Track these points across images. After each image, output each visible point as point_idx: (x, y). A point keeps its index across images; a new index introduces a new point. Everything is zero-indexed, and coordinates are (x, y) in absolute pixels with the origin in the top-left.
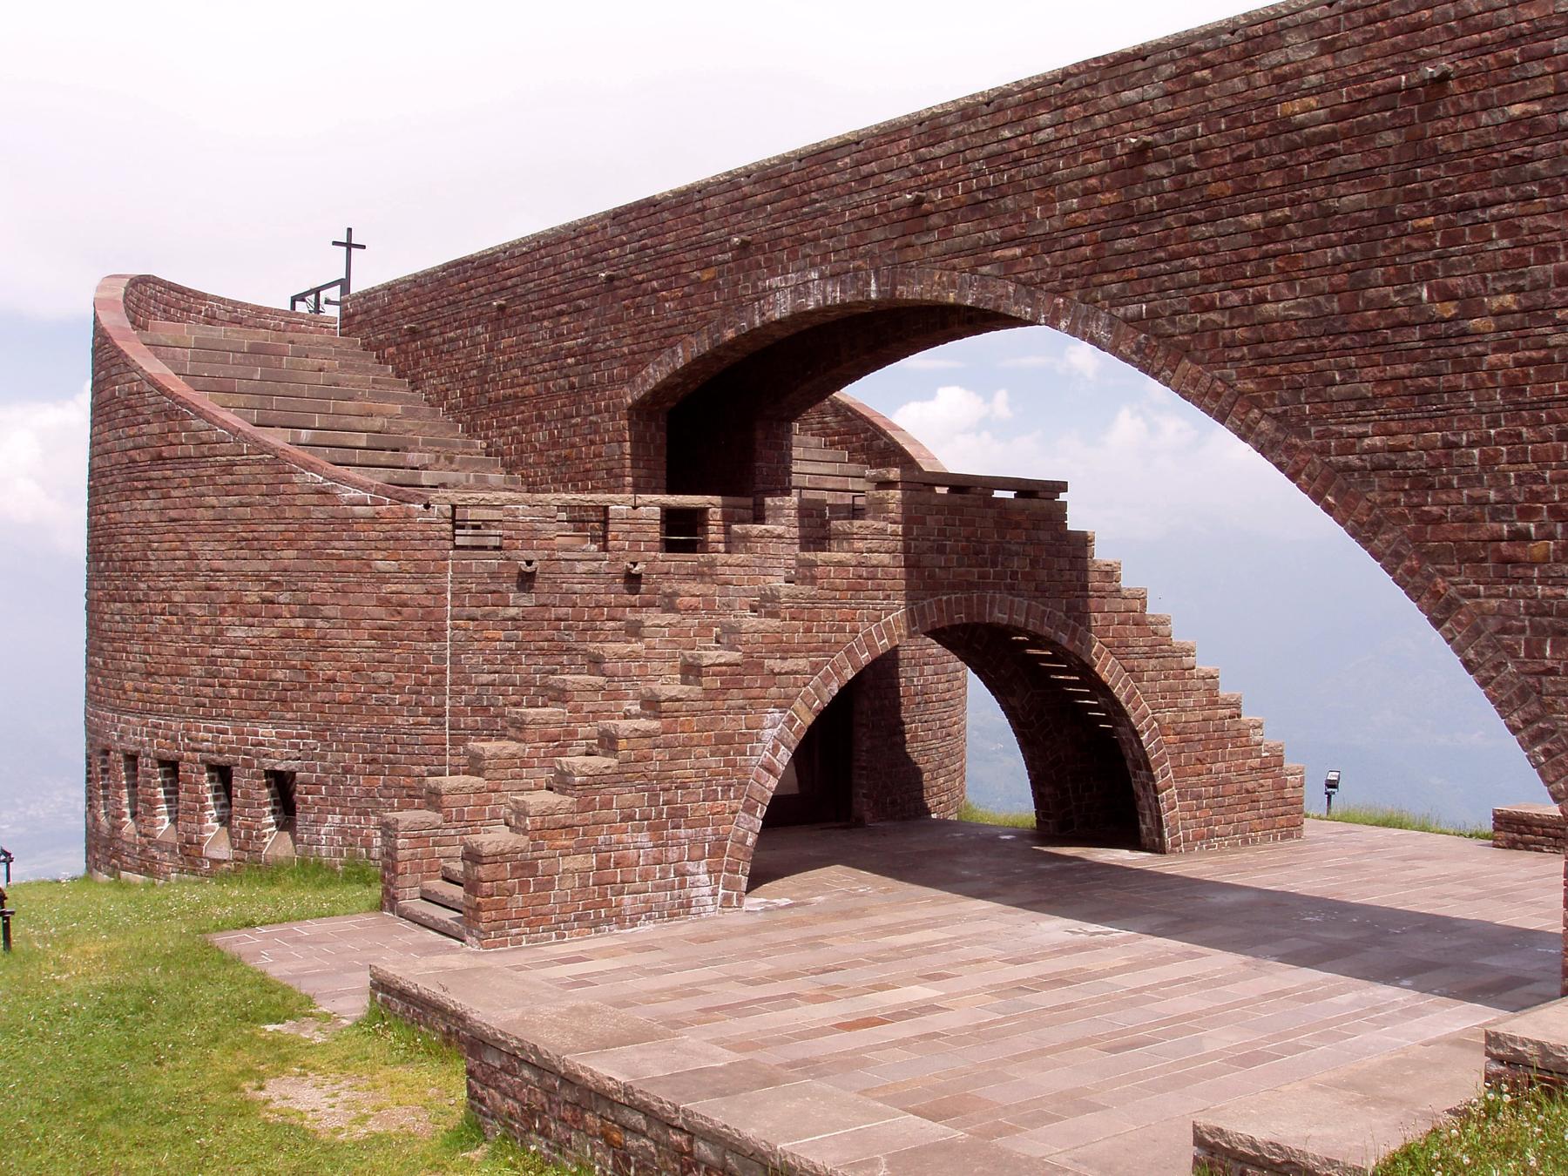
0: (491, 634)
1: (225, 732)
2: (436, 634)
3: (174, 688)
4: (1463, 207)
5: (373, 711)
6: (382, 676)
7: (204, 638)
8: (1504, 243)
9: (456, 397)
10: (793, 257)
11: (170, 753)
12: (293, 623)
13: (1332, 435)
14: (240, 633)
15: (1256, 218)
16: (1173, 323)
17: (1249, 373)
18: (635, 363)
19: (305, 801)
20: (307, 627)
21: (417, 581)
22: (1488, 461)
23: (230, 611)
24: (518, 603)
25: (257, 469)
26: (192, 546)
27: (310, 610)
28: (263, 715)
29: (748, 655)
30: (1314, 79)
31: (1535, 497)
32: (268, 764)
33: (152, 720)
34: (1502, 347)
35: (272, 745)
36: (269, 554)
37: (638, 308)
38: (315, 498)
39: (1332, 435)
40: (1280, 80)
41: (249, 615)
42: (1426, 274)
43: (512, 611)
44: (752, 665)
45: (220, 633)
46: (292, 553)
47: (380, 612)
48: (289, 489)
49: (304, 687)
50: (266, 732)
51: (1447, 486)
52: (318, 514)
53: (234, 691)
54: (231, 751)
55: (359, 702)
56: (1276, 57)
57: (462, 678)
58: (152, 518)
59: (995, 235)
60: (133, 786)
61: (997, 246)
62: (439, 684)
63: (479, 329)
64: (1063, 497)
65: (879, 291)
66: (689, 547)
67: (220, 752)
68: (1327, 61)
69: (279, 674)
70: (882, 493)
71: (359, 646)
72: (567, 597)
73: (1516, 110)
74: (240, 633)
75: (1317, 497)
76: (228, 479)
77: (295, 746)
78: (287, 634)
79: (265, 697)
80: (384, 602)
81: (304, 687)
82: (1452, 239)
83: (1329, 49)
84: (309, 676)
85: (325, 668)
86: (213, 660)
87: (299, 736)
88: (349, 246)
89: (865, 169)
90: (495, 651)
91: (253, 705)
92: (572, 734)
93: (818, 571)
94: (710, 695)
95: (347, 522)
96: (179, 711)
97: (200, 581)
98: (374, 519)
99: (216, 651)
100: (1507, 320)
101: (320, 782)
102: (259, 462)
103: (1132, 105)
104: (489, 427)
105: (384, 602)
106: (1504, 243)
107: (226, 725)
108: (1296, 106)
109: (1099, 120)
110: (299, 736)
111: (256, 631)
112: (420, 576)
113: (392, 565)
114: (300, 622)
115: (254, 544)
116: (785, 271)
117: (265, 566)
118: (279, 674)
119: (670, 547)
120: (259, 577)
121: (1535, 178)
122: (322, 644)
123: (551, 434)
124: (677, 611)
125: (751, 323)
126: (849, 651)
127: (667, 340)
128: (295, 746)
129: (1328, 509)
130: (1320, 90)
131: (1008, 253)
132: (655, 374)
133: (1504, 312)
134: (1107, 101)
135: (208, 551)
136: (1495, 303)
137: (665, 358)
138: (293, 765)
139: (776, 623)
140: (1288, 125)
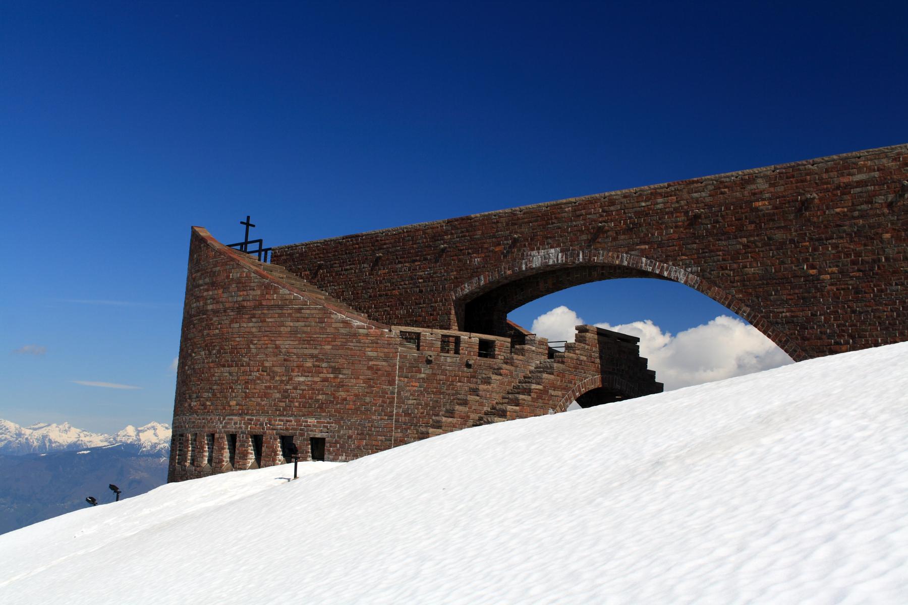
0: (414, 384)
1: (291, 421)
2: (391, 383)
3: (263, 403)
4: (820, 239)
5: (362, 413)
6: (368, 399)
7: (282, 381)
8: (833, 252)
9: (349, 294)
10: (542, 244)
11: (258, 431)
12: (328, 376)
13: (771, 312)
14: (302, 379)
15: (745, 240)
16: (710, 274)
17: (740, 291)
18: (458, 282)
19: (329, 450)
20: (335, 378)
21: (385, 360)
22: (827, 320)
23: (297, 370)
24: (425, 371)
25: (313, 312)
26: (277, 342)
27: (336, 370)
28: (310, 414)
29: (544, 387)
30: (767, 195)
31: (843, 331)
32: (312, 435)
33: (247, 417)
34: (832, 284)
35: (314, 426)
36: (319, 347)
37: (460, 260)
38: (341, 325)
39: (771, 312)
40: (754, 194)
41: (304, 371)
42: (806, 260)
43: (423, 376)
44: (545, 391)
45: (291, 379)
46: (329, 347)
47: (369, 373)
48: (329, 320)
49: (332, 402)
50: (311, 421)
51: (812, 328)
52: (342, 331)
53: (297, 404)
54: (293, 429)
55: (357, 409)
56: (753, 187)
57: (401, 401)
58: (254, 330)
59: (637, 240)
60: (211, 451)
61: (638, 244)
62: (392, 402)
63: (365, 265)
64: (638, 344)
65: (583, 258)
66: (486, 356)
67: (287, 429)
68: (772, 189)
69: (320, 397)
70: (583, 334)
71: (358, 386)
72: (444, 372)
73: (838, 210)
74: (302, 379)
75: (765, 332)
76: (298, 315)
77: (326, 427)
78: (325, 380)
79: (312, 406)
80: (370, 368)
81: (332, 402)
82: (815, 249)
83: (771, 185)
84: (334, 398)
85: (342, 394)
86: (286, 391)
87: (328, 423)
88: (248, 224)
89: (578, 213)
90: (414, 391)
91: (306, 410)
92: (469, 417)
93: (565, 360)
94: (534, 400)
95: (355, 335)
96: (265, 413)
97: (282, 357)
98: (367, 335)
99: (288, 387)
100: (834, 276)
101: (337, 442)
102: (315, 309)
103: (697, 199)
104: (370, 307)
105: (370, 368)
106: (833, 252)
107: (291, 418)
108: (760, 204)
109: (683, 203)
110: (328, 423)
111: (309, 379)
112: (387, 358)
113: (374, 354)
114: (332, 376)
115: (309, 341)
116: (538, 249)
117: (316, 352)
118: (320, 397)
119: (480, 355)
120: (312, 356)
121: (845, 231)
122: (341, 385)
123: (408, 312)
124: (501, 375)
125: (520, 268)
126: (573, 391)
127: (476, 272)
128: (326, 427)
129: (769, 336)
130: (770, 199)
131: (643, 247)
132: (467, 289)
133: (833, 273)
134: (686, 196)
135: (286, 344)
136: (830, 270)
137: (475, 280)
138: (324, 435)
139: (552, 376)
140: (757, 209)
